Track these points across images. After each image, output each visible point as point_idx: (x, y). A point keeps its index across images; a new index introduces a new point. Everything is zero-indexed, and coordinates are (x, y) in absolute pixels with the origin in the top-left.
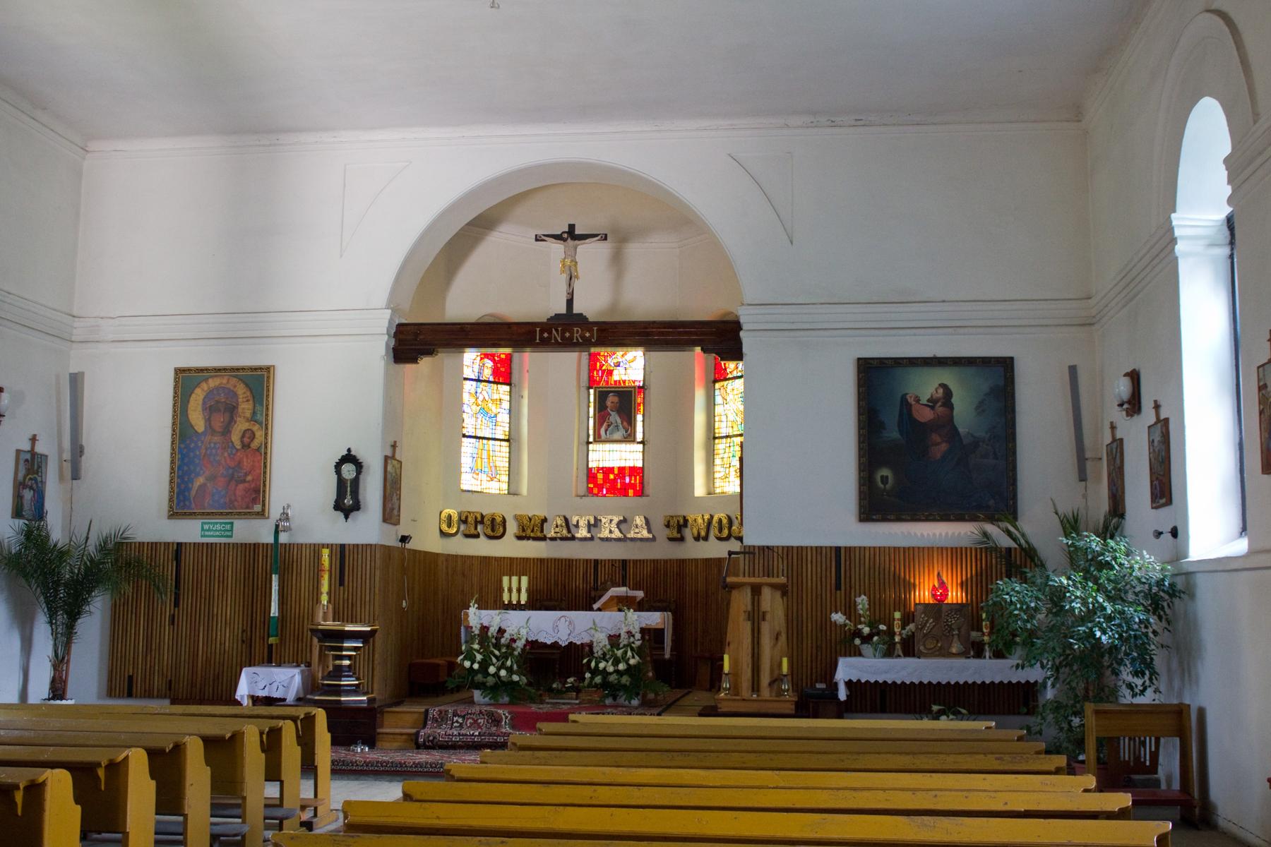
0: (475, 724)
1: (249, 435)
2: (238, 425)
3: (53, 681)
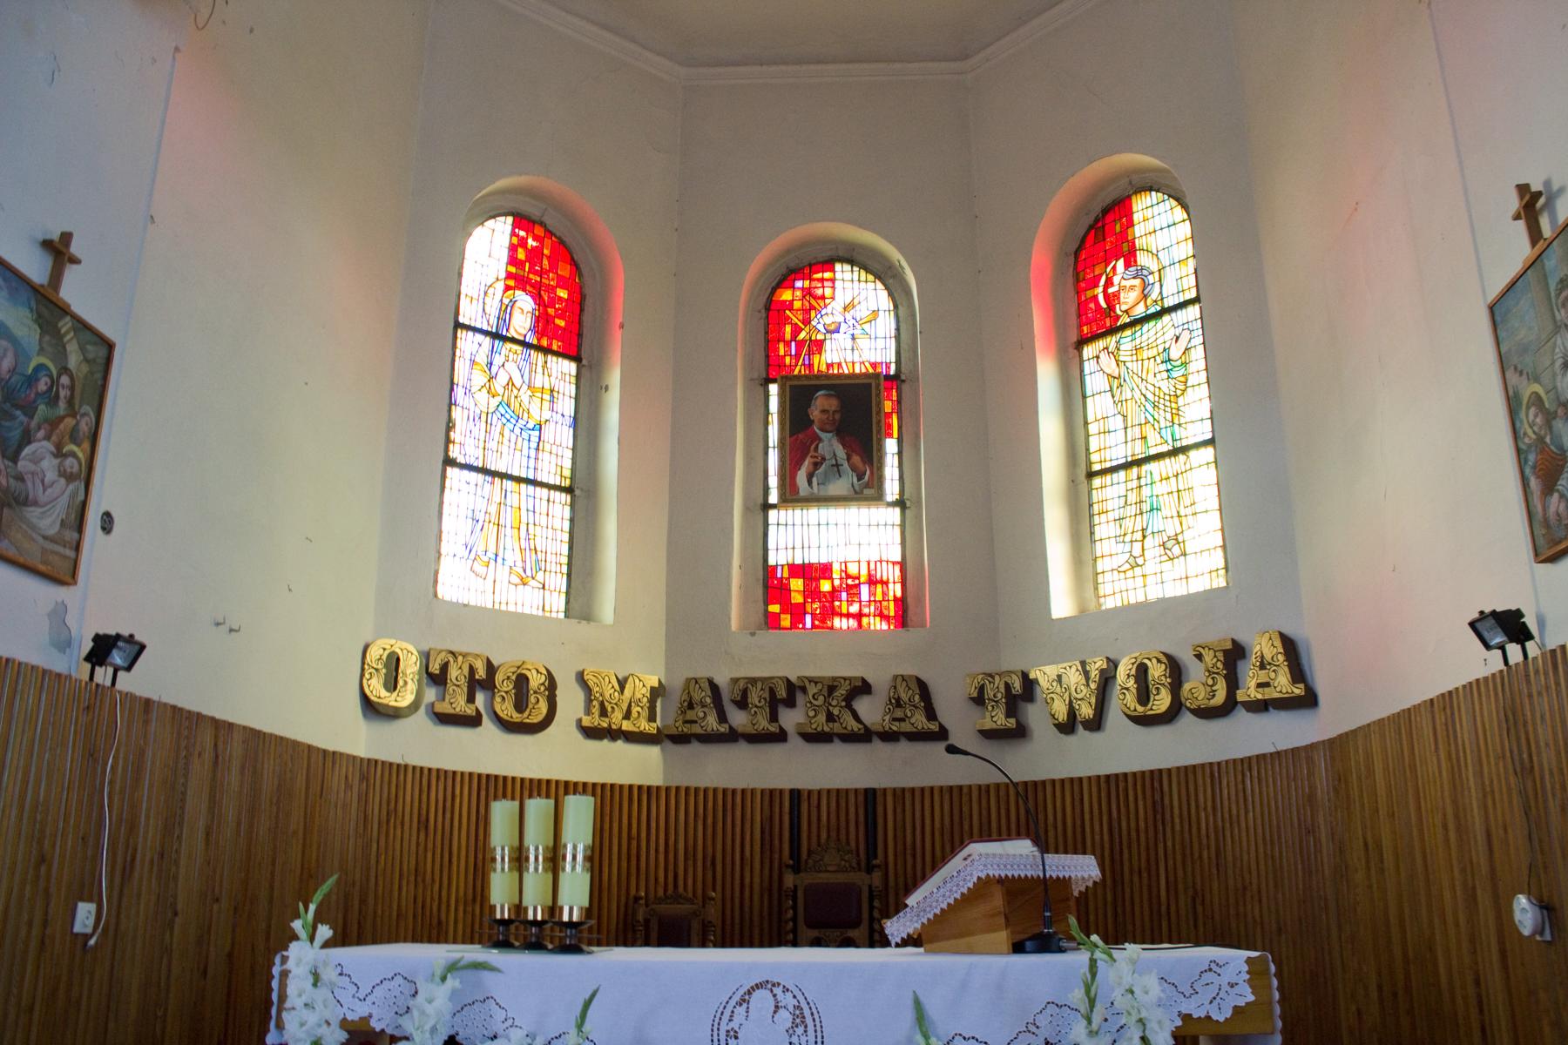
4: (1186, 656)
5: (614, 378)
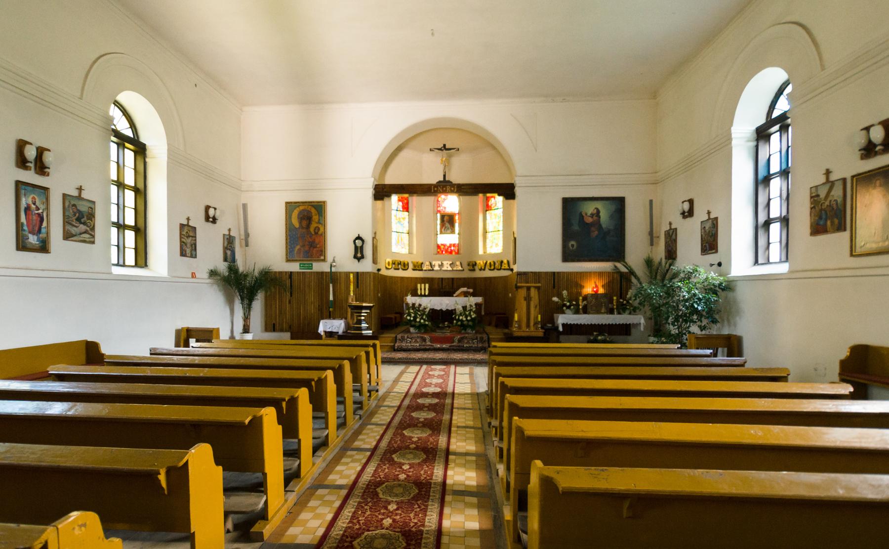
0: (416, 342)
3: (244, 326)
4: (496, 261)
5: (415, 216)
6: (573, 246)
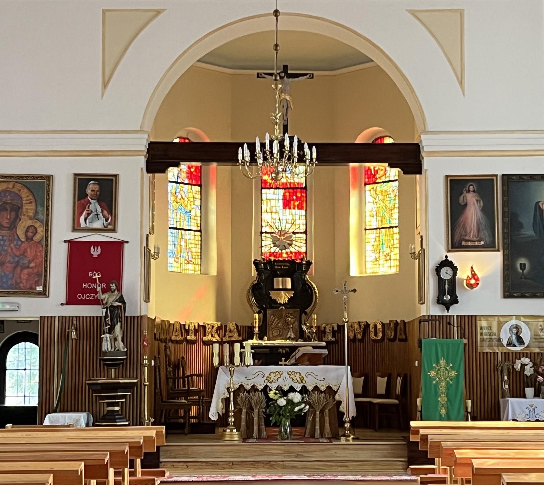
1: (31, 230)
2: (22, 222)
6: (523, 266)
